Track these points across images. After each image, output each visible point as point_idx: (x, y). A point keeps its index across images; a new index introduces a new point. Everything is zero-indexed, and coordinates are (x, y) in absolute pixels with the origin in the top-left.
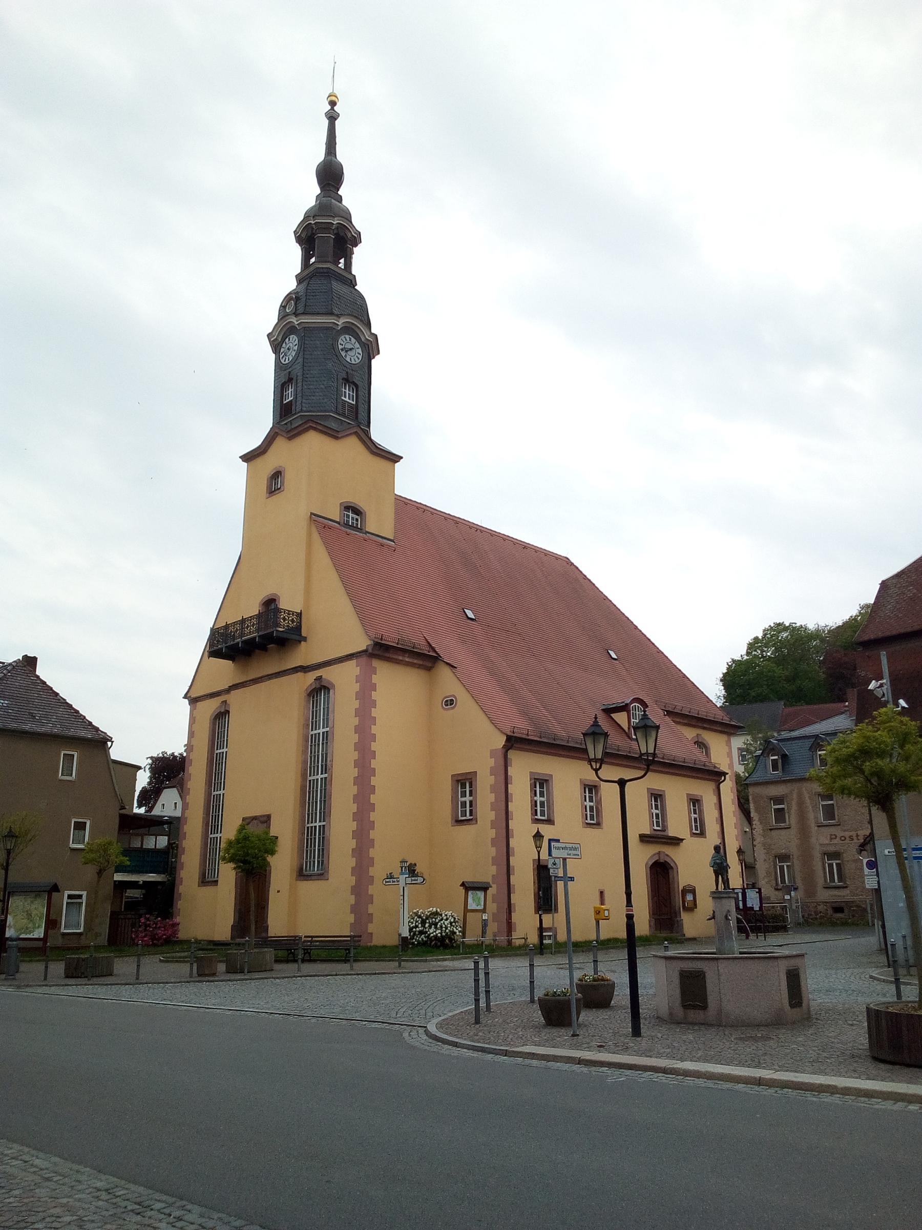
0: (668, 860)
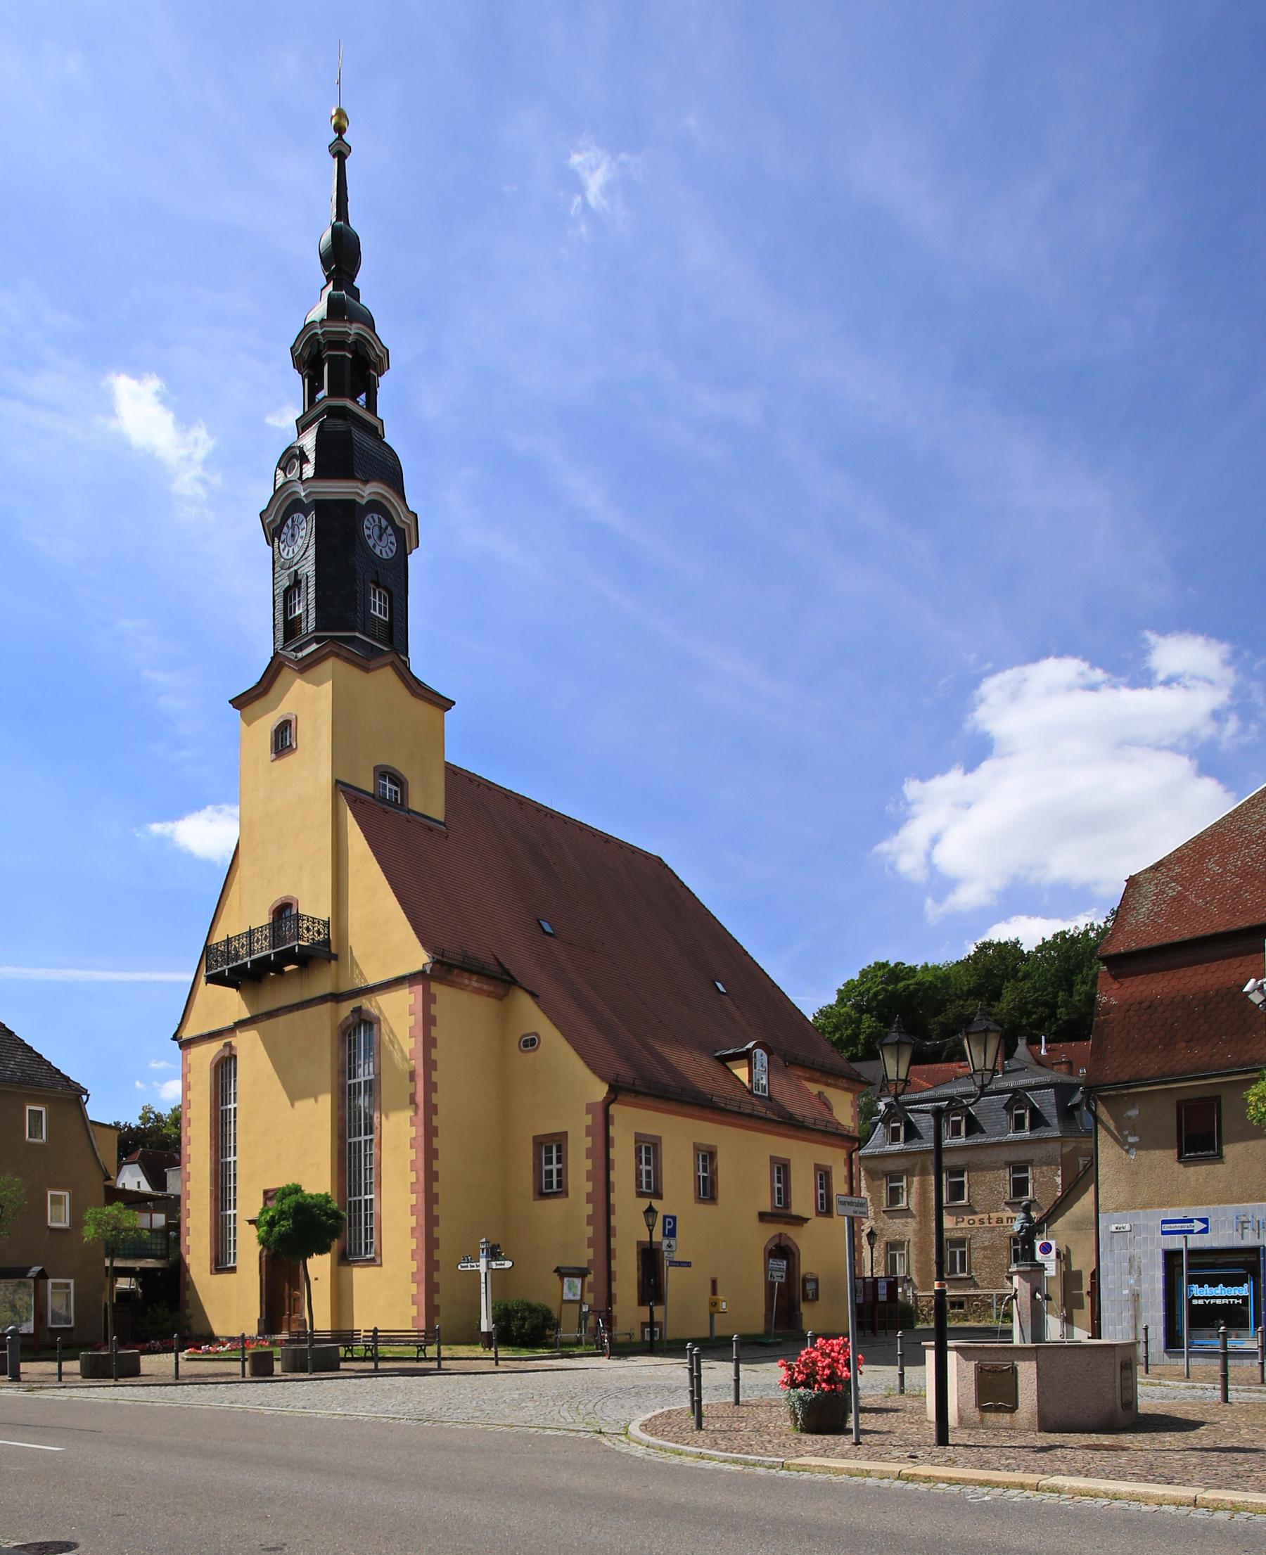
0: (790, 1244)
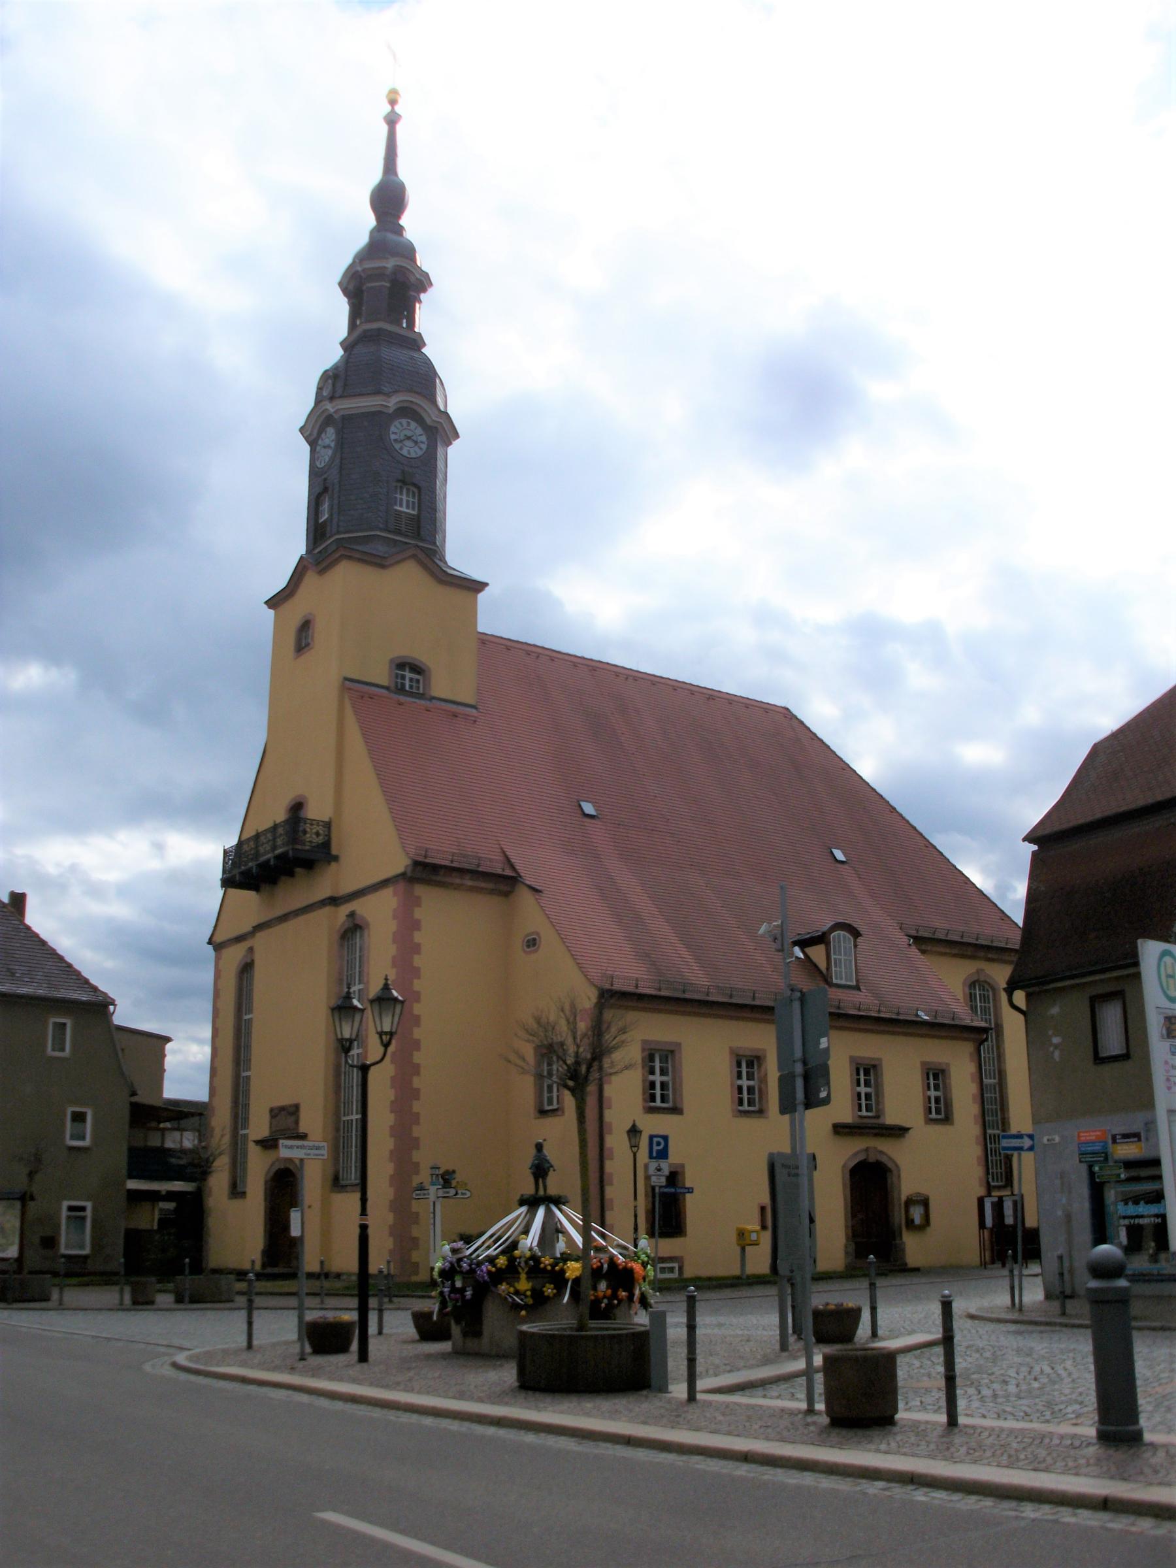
0: (884, 1159)
